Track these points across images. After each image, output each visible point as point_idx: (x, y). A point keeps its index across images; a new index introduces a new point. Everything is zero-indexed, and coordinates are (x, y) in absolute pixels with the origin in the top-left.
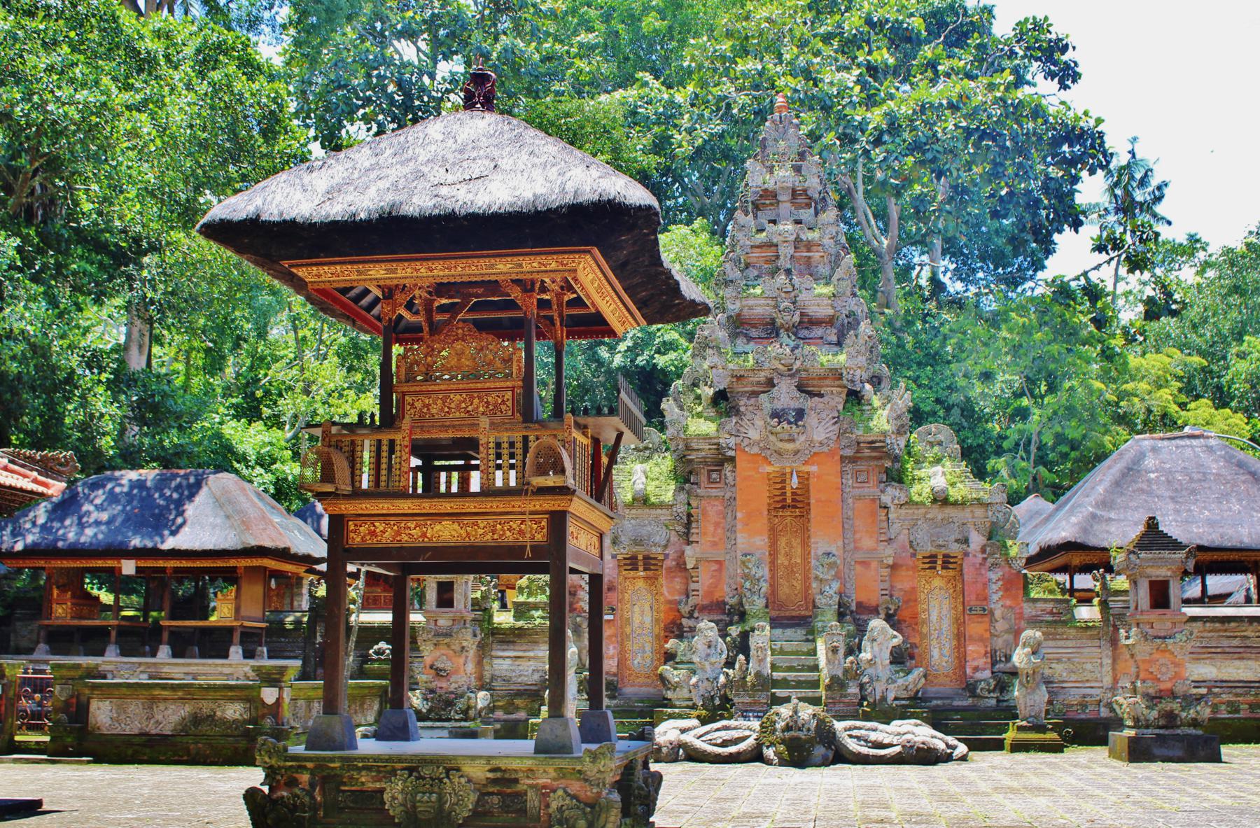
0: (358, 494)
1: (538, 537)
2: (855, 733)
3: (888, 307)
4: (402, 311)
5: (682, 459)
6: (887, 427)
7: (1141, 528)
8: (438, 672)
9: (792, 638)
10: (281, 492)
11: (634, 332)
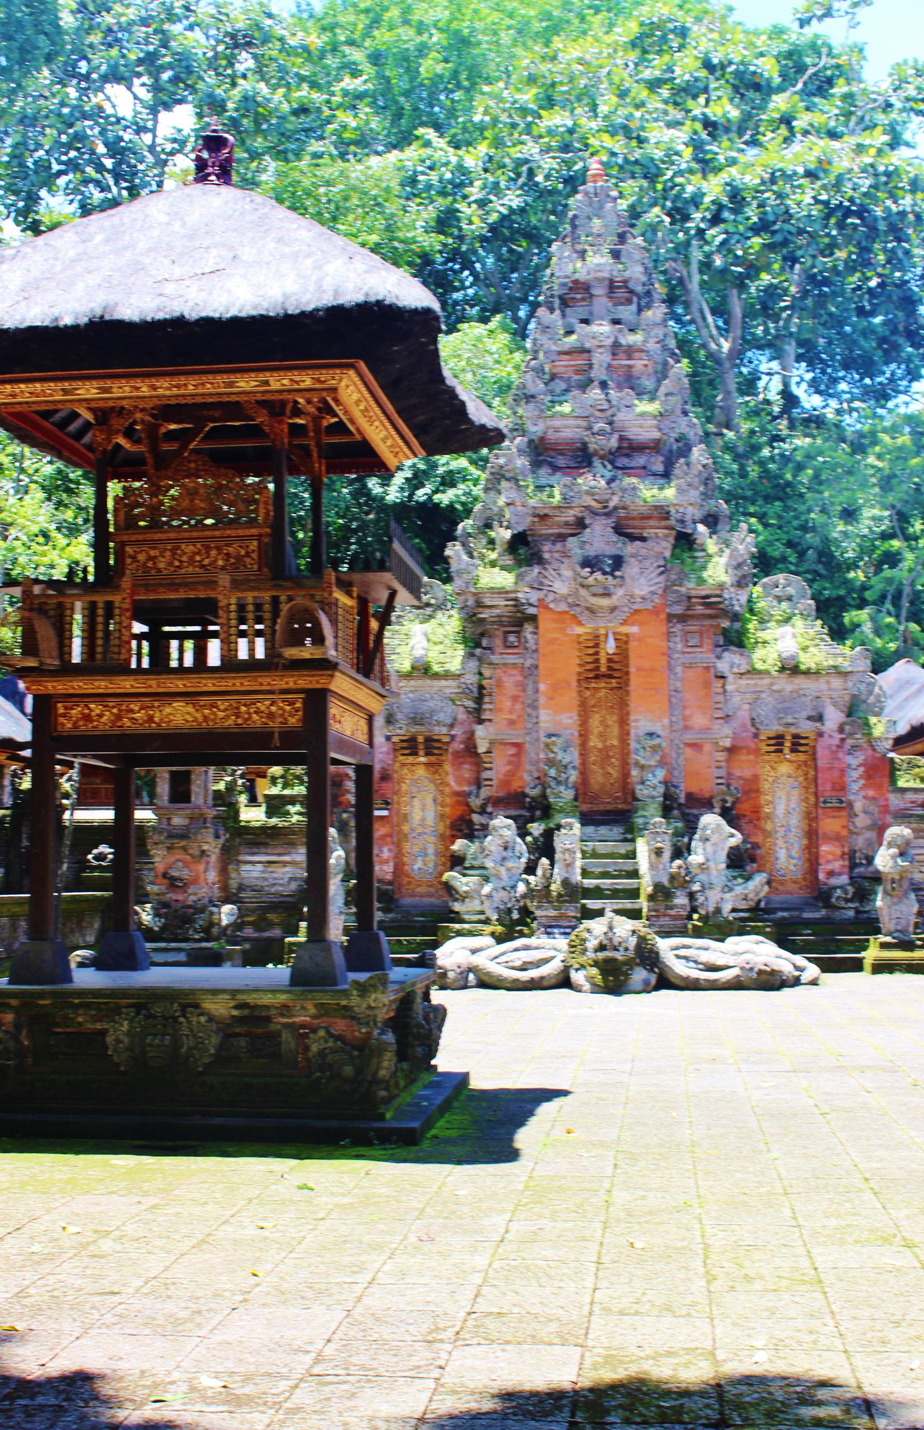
0: (67, 669)
1: (292, 721)
2: (682, 952)
3: (728, 427)
4: (121, 441)
8: (173, 883)
9: (607, 839)
11: (411, 463)
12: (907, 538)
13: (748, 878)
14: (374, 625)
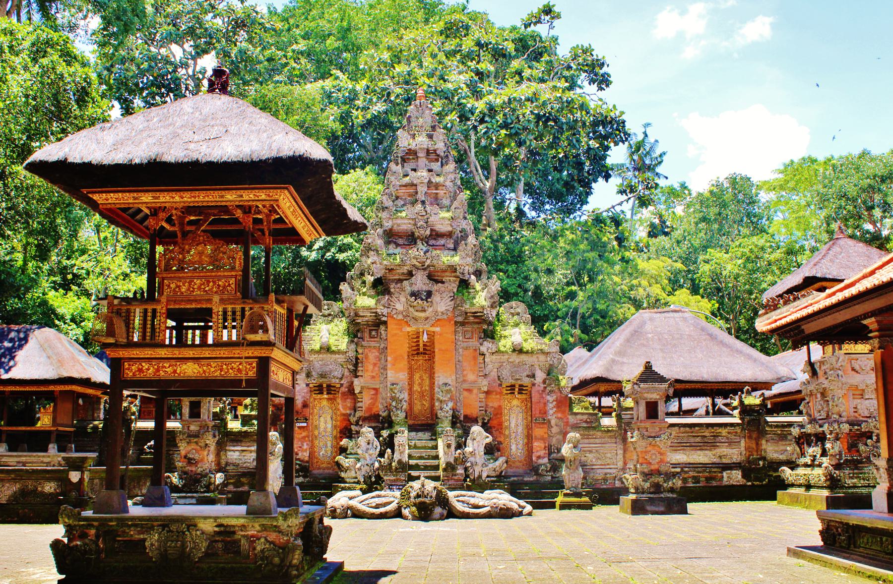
0: (131, 345)
1: (251, 374)
2: (461, 499)
5: (353, 322)
6: (484, 303)
7: (641, 369)
8: (190, 461)
9: (423, 437)
10: (86, 343)
12: (580, 285)
13: (496, 460)
14: (296, 323)
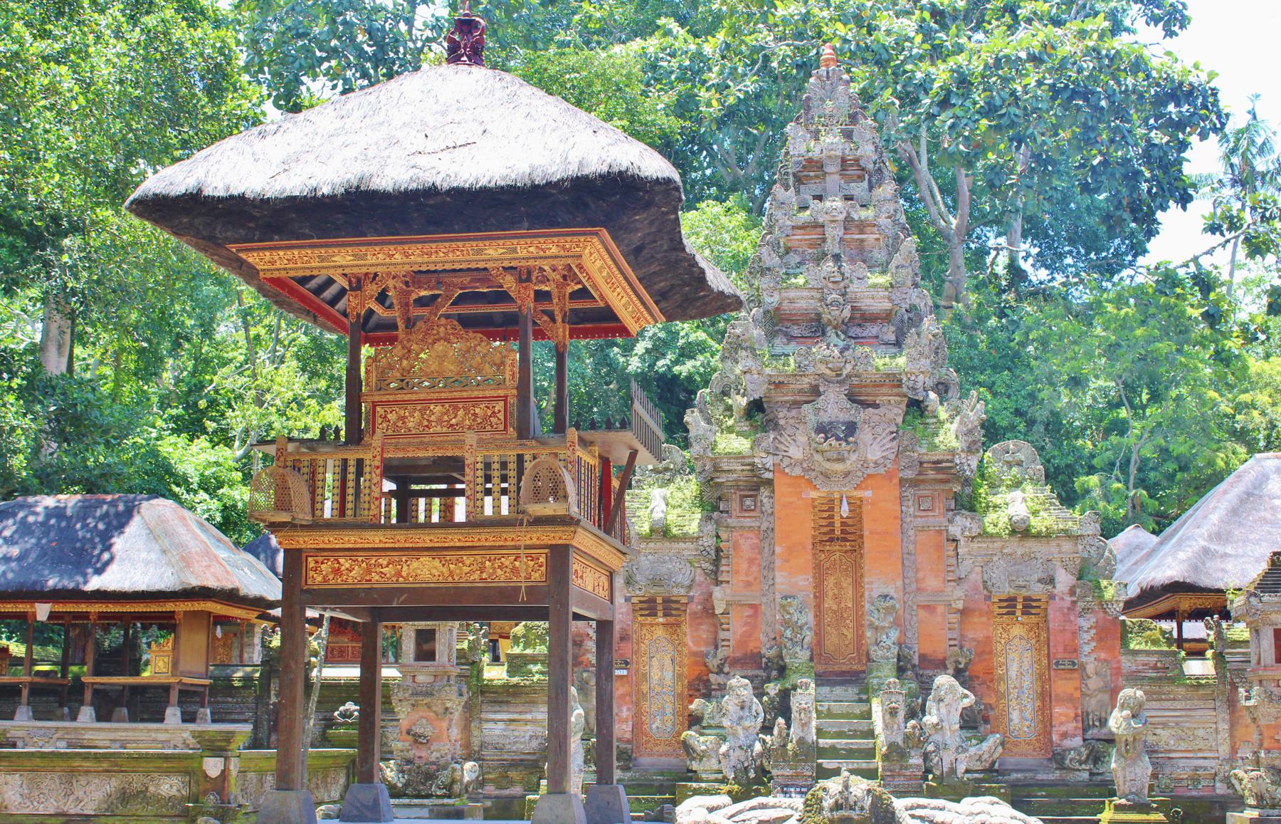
0: (319, 525)
1: (535, 576)
2: (918, 812)
5: (709, 482)
8: (418, 739)
10: (229, 522)
